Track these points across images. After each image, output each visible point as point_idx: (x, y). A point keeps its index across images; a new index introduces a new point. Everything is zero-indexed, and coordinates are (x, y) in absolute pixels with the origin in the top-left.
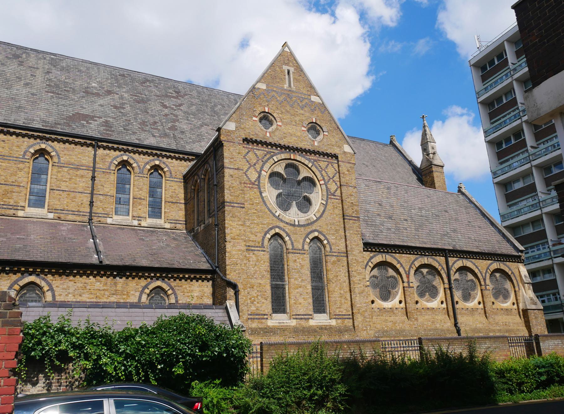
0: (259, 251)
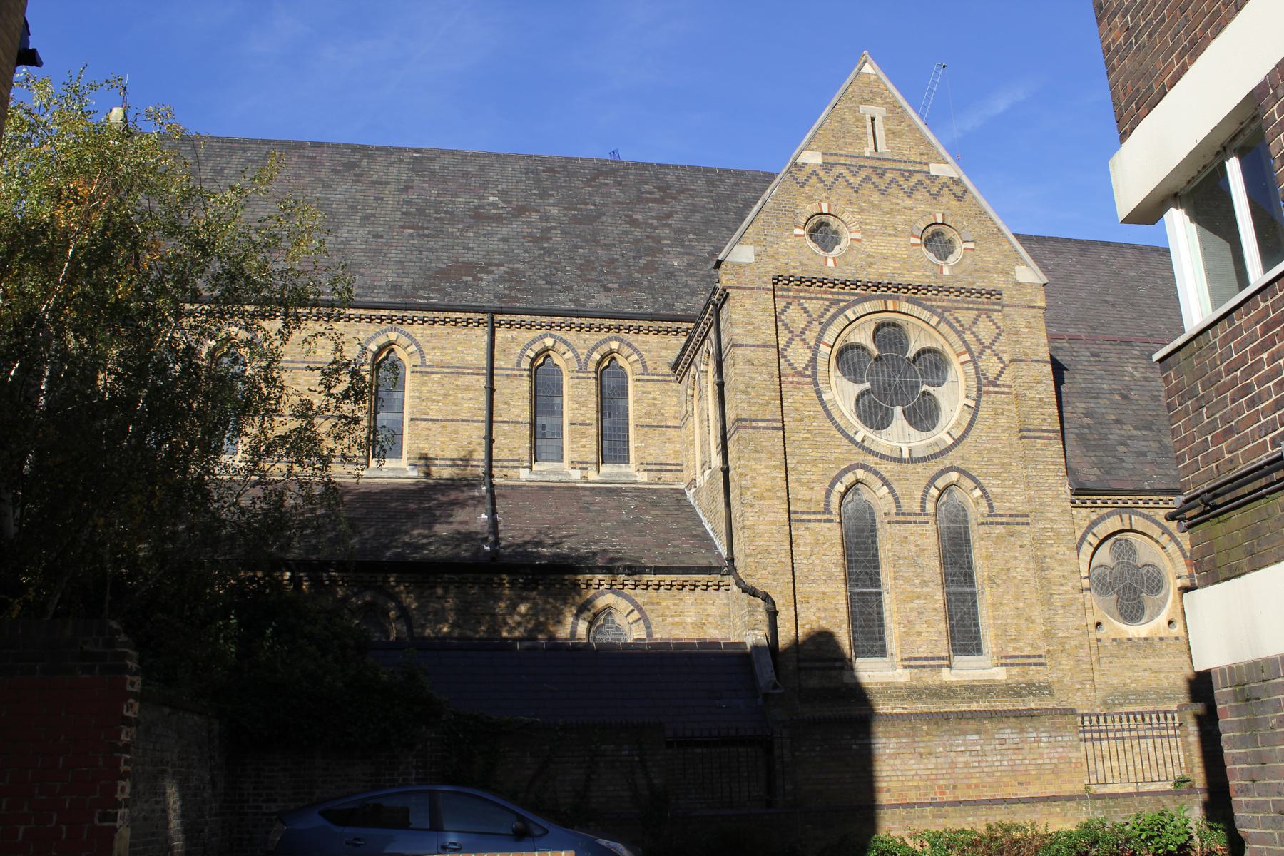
0: (820, 521)
